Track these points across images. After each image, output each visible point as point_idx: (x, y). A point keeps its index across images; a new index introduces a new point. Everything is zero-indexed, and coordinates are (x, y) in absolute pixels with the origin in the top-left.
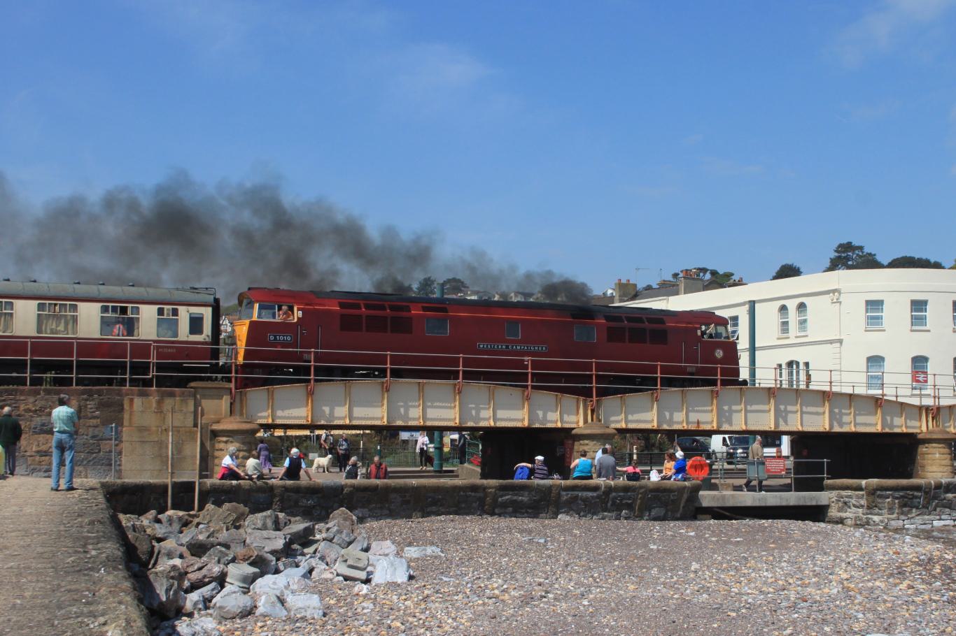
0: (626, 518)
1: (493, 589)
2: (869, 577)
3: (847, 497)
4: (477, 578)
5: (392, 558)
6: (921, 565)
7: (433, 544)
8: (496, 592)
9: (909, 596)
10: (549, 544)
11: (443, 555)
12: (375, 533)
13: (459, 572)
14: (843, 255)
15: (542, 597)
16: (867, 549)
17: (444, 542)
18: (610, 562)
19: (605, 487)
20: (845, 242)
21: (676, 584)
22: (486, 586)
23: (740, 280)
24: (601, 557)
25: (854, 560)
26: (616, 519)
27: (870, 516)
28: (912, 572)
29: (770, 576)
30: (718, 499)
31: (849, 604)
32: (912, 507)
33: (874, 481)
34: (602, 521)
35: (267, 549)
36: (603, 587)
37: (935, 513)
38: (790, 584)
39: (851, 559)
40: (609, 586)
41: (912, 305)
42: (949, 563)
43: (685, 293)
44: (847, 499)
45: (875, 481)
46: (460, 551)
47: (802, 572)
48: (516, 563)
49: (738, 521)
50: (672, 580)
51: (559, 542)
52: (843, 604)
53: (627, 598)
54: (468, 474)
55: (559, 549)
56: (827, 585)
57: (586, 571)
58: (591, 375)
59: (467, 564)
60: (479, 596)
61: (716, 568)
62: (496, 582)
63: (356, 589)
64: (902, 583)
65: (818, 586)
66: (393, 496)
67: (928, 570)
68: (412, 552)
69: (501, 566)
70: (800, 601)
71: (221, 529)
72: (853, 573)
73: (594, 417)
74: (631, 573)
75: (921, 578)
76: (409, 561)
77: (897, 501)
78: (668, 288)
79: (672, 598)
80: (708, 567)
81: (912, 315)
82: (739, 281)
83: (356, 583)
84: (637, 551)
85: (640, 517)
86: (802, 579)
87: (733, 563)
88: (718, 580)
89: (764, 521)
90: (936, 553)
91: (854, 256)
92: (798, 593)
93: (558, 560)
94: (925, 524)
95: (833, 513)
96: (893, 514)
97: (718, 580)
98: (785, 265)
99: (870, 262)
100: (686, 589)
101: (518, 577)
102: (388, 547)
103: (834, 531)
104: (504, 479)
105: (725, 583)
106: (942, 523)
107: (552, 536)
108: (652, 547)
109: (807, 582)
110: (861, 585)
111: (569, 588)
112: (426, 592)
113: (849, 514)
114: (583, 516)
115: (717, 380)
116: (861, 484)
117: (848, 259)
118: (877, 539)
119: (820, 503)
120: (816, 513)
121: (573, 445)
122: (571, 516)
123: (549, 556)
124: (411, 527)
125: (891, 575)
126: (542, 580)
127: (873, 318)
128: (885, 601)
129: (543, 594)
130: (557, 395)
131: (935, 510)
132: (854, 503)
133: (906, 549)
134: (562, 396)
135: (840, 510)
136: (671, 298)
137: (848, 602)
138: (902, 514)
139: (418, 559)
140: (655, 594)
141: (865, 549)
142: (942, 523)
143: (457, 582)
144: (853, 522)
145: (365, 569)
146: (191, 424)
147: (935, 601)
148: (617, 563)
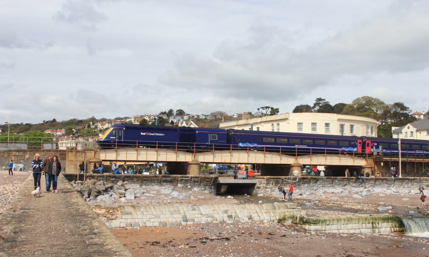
20: (319, 98)
35: (101, 190)
45: (268, 177)
71: (90, 185)
127: (299, 128)
135: (259, 184)
146: (84, 160)
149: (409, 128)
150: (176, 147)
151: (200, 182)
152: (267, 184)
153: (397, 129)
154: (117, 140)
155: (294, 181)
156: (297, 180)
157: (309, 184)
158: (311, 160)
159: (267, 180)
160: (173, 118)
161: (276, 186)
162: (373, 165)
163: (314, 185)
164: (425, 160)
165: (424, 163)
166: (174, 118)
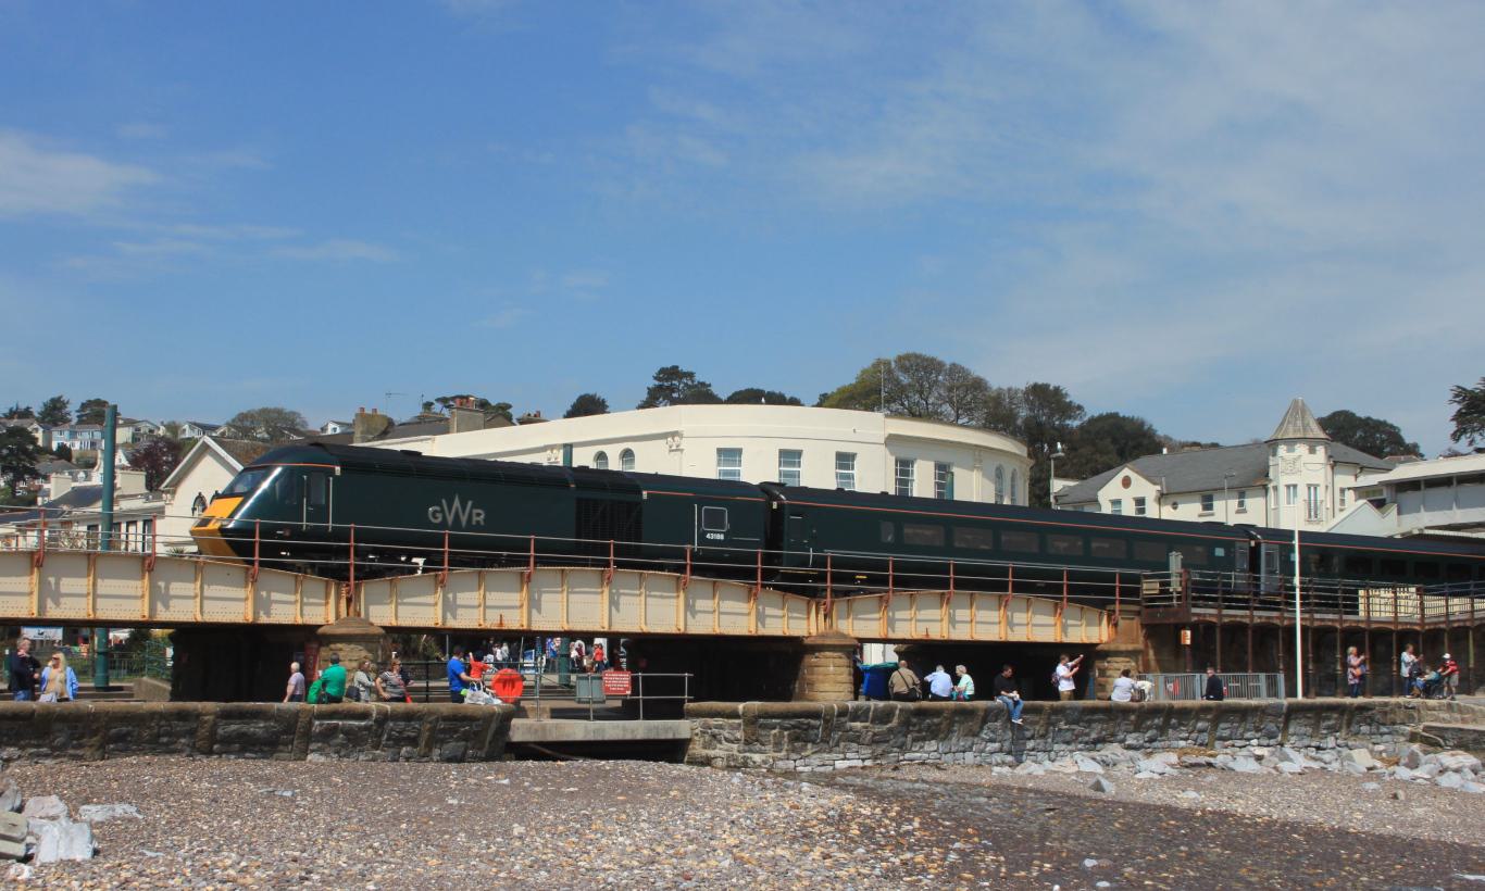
0: (407, 759)
1: (225, 869)
2: (766, 842)
3: (717, 727)
4: (198, 852)
5: (64, 822)
6: (831, 825)
7: (123, 800)
8: (232, 872)
9: (829, 869)
10: (299, 798)
11: (141, 817)
12: (31, 784)
13: (168, 843)
14: (666, 384)
15: (303, 879)
16: (753, 803)
17: (139, 796)
18: (394, 825)
19: (378, 714)
21: (496, 856)
22: (214, 863)
23: (538, 415)
24: (380, 818)
25: (739, 817)
26: (394, 760)
27: (748, 754)
28: (821, 835)
29: (628, 842)
30: (536, 731)
31: (750, 883)
32: (807, 742)
33: (756, 705)
34: (373, 764)
36: (391, 863)
37: (837, 749)
38: (658, 854)
39: (735, 816)
40: (400, 861)
41: (780, 457)
42: (868, 821)
43: (458, 431)
44: (716, 731)
46: (166, 811)
47: (671, 836)
48: (254, 828)
49: (568, 762)
50: (490, 851)
51: (313, 796)
52: (742, 882)
53: (431, 879)
54: (150, 694)
55: (314, 806)
56: (710, 854)
57: (360, 838)
58: (686, 565)
59: (180, 829)
60: (206, 879)
61: (549, 832)
62: (227, 857)
63: (12, 872)
64: (811, 851)
65: (697, 854)
66: (58, 726)
67: (843, 830)
68: (95, 812)
69: (232, 833)
70: (680, 879)
72: (742, 837)
73: (352, 609)
74: (428, 840)
75: (837, 843)
76: (92, 825)
77: (786, 733)
78: (430, 423)
79: (496, 877)
80: (537, 830)
81: (780, 472)
82: (535, 416)
83: (10, 862)
84: (431, 808)
85: (425, 756)
86: (673, 847)
87: (572, 824)
88: (556, 849)
89: (603, 762)
90: (847, 807)
91: (682, 385)
92: (675, 868)
93: (315, 823)
94: (823, 765)
95: (697, 750)
96: (780, 751)
97: (556, 849)
98: (586, 395)
99: (703, 395)
100: (513, 865)
101: (260, 849)
102: (53, 804)
103: (701, 776)
104: (226, 701)
105: (566, 854)
106: (847, 764)
107: (301, 786)
108: (450, 802)
109: (682, 850)
110: (757, 854)
111: (340, 866)
112: (124, 875)
113: (719, 751)
114: (345, 756)
115: (529, 557)
116: (737, 709)
117: (672, 389)
118: (764, 788)
119: (678, 737)
120: (672, 751)
121: (318, 651)
122: (327, 755)
123: (302, 817)
124: (86, 774)
125: (794, 839)
126: (297, 854)
128: (799, 877)
129: (303, 874)
130: (296, 576)
131: (837, 745)
132: (727, 735)
133: (805, 801)
134: (305, 577)
136: (438, 438)
137: (748, 879)
138: (793, 751)
139: (102, 823)
140: (471, 873)
141: (752, 802)
142: (847, 764)
143: (169, 858)
144: (725, 763)
145: (23, 840)
147: (865, 876)
148: (404, 826)
149: (1126, 482)
150: (1062, 585)
151: (430, 746)
152: (747, 742)
153: (1069, 487)
154: (330, 524)
155: (878, 729)
156: (895, 722)
157: (943, 739)
158: (534, 604)
159: (752, 721)
160: (67, 433)
161: (794, 756)
162: (1142, 639)
163: (969, 743)
164: (1345, 617)
165: (1344, 631)
166: (73, 435)
